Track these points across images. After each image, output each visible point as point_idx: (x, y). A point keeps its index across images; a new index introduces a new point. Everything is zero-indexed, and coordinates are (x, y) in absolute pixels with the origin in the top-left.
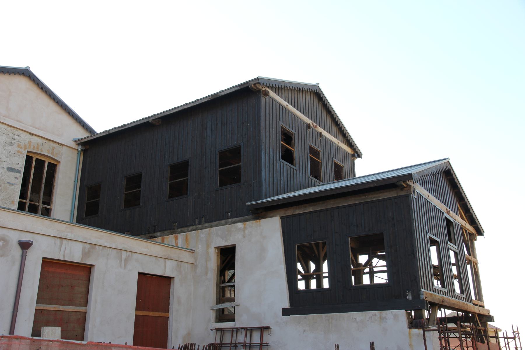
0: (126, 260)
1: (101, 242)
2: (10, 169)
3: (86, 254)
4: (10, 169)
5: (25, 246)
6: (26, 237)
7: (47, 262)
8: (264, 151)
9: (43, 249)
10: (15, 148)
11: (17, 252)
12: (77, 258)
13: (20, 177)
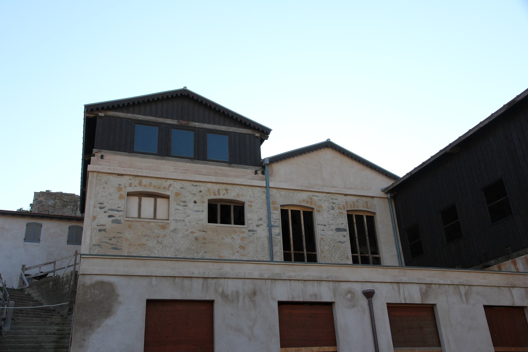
0: (466, 295)
1: (436, 280)
2: (338, 230)
3: (424, 294)
4: (338, 230)
5: (369, 295)
6: (368, 287)
7: (392, 308)
8: (324, 276)
9: (385, 296)
10: (337, 211)
11: (364, 301)
12: (417, 299)
13: (347, 234)
